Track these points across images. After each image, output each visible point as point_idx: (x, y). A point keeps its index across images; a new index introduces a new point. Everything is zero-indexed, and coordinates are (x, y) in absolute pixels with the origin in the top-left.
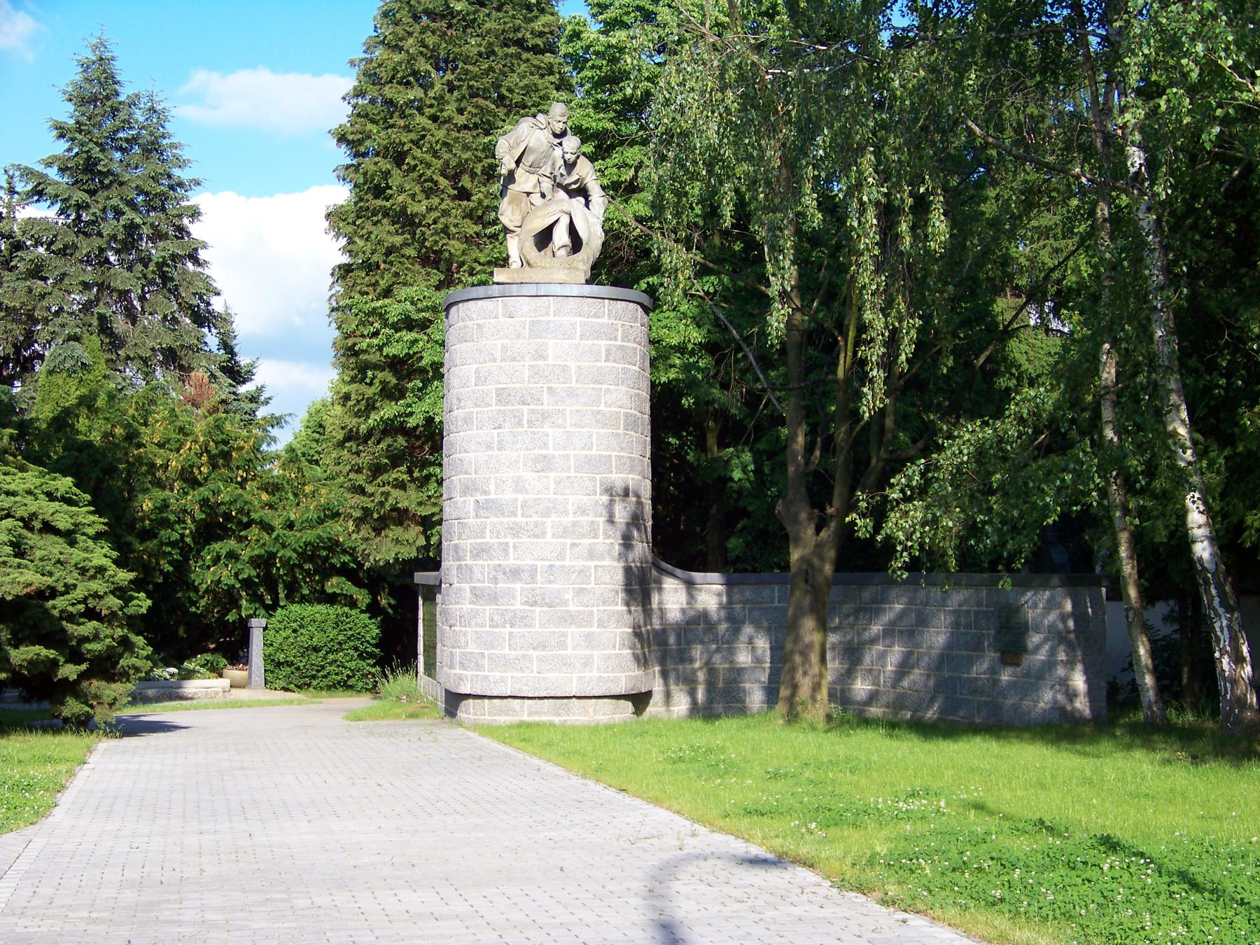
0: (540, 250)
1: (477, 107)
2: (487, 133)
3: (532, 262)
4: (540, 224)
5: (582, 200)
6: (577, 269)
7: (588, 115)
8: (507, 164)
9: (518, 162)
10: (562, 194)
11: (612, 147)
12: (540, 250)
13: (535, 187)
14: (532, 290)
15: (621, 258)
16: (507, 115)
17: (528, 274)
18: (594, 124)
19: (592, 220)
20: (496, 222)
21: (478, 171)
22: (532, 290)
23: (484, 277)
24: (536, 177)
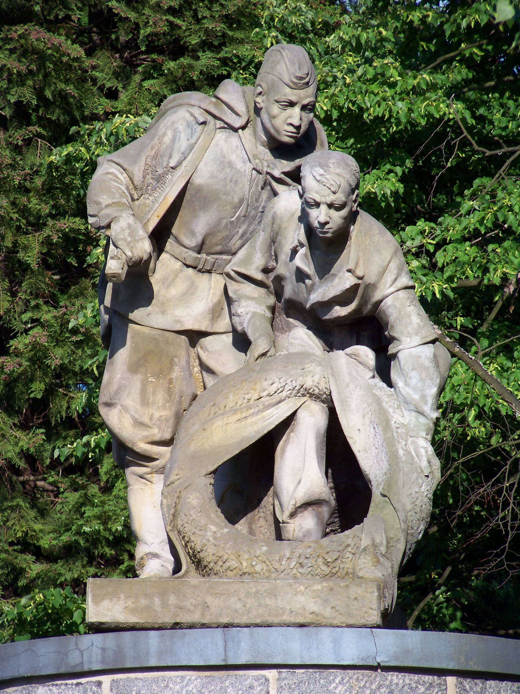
0: (233, 518)
1: (25, 52)
2: (60, 136)
3: (208, 556)
4: (232, 432)
5: (366, 354)
6: (353, 576)
7: (382, 79)
8: (126, 240)
9: (160, 236)
10: (301, 337)
11: (463, 176)
12: (233, 518)
13: (215, 313)
14: (208, 647)
15: (497, 537)
16: (123, 74)
17: (196, 598)
18: (401, 106)
19: (402, 417)
20: (88, 421)
21: (31, 257)
22: (208, 647)
23: (56, 597)
24: (217, 282)
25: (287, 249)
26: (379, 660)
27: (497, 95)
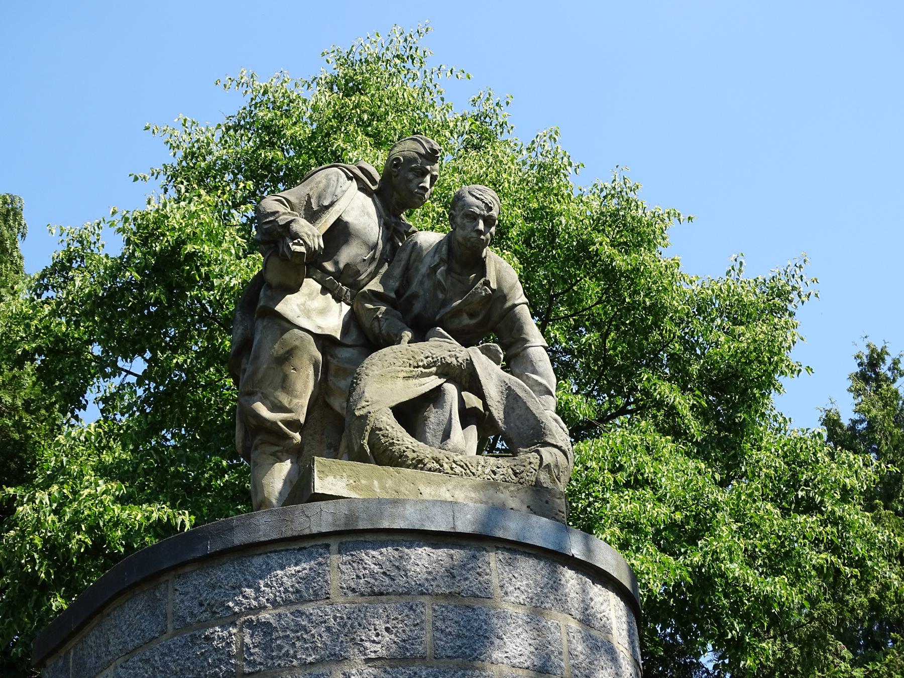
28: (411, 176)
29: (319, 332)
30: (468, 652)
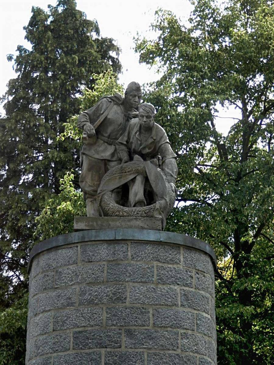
25: (133, 133)
26: (161, 240)
27: (216, 19)
28: (131, 98)
29: (102, 158)
30: (118, 279)
